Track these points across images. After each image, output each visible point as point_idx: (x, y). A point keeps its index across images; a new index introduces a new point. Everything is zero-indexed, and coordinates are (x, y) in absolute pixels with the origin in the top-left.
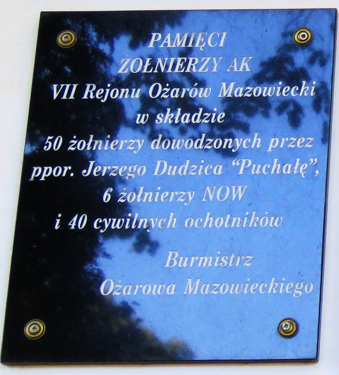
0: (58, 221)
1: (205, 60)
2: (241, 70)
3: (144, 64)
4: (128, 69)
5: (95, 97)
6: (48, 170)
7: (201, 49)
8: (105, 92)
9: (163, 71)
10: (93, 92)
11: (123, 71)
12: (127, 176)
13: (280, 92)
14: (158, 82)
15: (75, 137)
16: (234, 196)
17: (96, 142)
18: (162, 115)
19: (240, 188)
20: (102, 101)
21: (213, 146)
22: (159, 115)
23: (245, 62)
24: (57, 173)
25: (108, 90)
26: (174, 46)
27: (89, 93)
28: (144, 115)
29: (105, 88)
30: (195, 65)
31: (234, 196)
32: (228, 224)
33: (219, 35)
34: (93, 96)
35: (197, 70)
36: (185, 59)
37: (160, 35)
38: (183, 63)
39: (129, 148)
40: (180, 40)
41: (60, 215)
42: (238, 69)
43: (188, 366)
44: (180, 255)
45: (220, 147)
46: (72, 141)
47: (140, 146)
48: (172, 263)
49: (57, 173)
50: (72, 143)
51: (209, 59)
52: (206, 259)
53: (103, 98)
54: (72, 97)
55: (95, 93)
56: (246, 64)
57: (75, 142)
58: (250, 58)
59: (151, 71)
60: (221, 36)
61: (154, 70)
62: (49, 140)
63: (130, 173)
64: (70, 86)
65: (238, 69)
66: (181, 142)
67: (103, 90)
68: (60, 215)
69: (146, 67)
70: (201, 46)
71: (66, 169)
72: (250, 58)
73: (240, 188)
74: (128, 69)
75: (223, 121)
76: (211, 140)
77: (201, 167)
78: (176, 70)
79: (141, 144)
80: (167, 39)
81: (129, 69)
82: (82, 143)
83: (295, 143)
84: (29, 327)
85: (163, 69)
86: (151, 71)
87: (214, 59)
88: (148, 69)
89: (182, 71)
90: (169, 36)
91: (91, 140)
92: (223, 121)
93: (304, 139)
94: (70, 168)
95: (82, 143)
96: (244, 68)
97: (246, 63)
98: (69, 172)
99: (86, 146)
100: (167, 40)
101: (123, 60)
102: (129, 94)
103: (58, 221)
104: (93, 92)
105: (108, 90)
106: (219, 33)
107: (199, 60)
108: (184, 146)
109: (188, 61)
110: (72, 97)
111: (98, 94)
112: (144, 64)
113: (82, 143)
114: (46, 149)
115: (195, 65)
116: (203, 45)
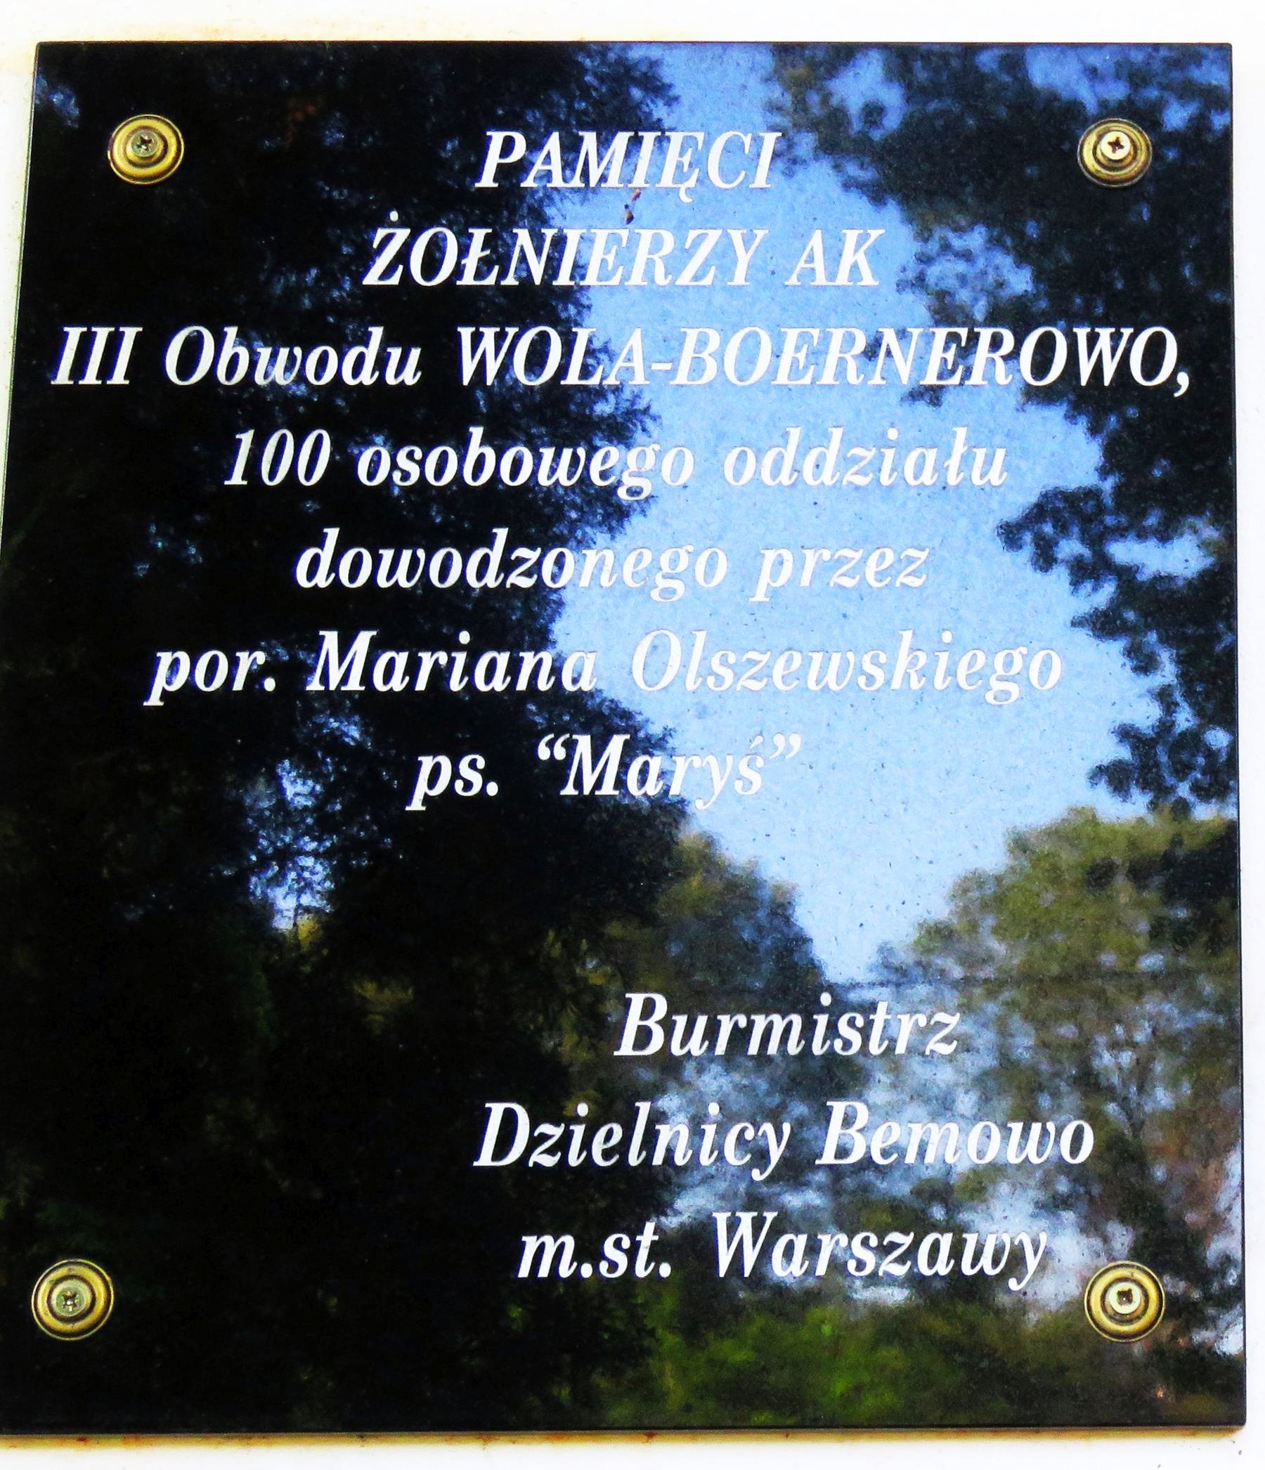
2: (843, 278)
3: (463, 251)
4: (401, 268)
7: (685, 198)
9: (537, 281)
11: (382, 277)
12: (989, 689)
14: (199, 324)
18: (418, 454)
21: (863, 578)
22: (406, 450)
23: (856, 251)
24: (209, 679)
28: (567, 453)
30: (664, 258)
33: (747, 140)
35: (670, 277)
37: (520, 141)
39: (836, 579)
42: (832, 276)
43: (270, 1444)
44: (673, 1010)
45: (453, 582)
48: (644, 1036)
49: (209, 679)
51: (714, 236)
52: (779, 1023)
54: (119, 378)
56: (862, 260)
59: (491, 280)
61: (503, 274)
63: (1000, 679)
65: (832, 276)
66: (414, 561)
69: (471, 264)
70: (683, 187)
74: (401, 268)
76: (531, 555)
77: (944, 658)
81: (407, 274)
82: (449, 557)
84: (48, 1291)
85: (537, 270)
86: (491, 280)
87: (737, 236)
90: (553, 143)
93: (890, 557)
94: (261, 657)
98: (255, 677)
101: (381, 233)
106: (750, 136)
107: (680, 239)
110: (119, 378)
112: (463, 251)
115: (664, 258)
116: (692, 182)
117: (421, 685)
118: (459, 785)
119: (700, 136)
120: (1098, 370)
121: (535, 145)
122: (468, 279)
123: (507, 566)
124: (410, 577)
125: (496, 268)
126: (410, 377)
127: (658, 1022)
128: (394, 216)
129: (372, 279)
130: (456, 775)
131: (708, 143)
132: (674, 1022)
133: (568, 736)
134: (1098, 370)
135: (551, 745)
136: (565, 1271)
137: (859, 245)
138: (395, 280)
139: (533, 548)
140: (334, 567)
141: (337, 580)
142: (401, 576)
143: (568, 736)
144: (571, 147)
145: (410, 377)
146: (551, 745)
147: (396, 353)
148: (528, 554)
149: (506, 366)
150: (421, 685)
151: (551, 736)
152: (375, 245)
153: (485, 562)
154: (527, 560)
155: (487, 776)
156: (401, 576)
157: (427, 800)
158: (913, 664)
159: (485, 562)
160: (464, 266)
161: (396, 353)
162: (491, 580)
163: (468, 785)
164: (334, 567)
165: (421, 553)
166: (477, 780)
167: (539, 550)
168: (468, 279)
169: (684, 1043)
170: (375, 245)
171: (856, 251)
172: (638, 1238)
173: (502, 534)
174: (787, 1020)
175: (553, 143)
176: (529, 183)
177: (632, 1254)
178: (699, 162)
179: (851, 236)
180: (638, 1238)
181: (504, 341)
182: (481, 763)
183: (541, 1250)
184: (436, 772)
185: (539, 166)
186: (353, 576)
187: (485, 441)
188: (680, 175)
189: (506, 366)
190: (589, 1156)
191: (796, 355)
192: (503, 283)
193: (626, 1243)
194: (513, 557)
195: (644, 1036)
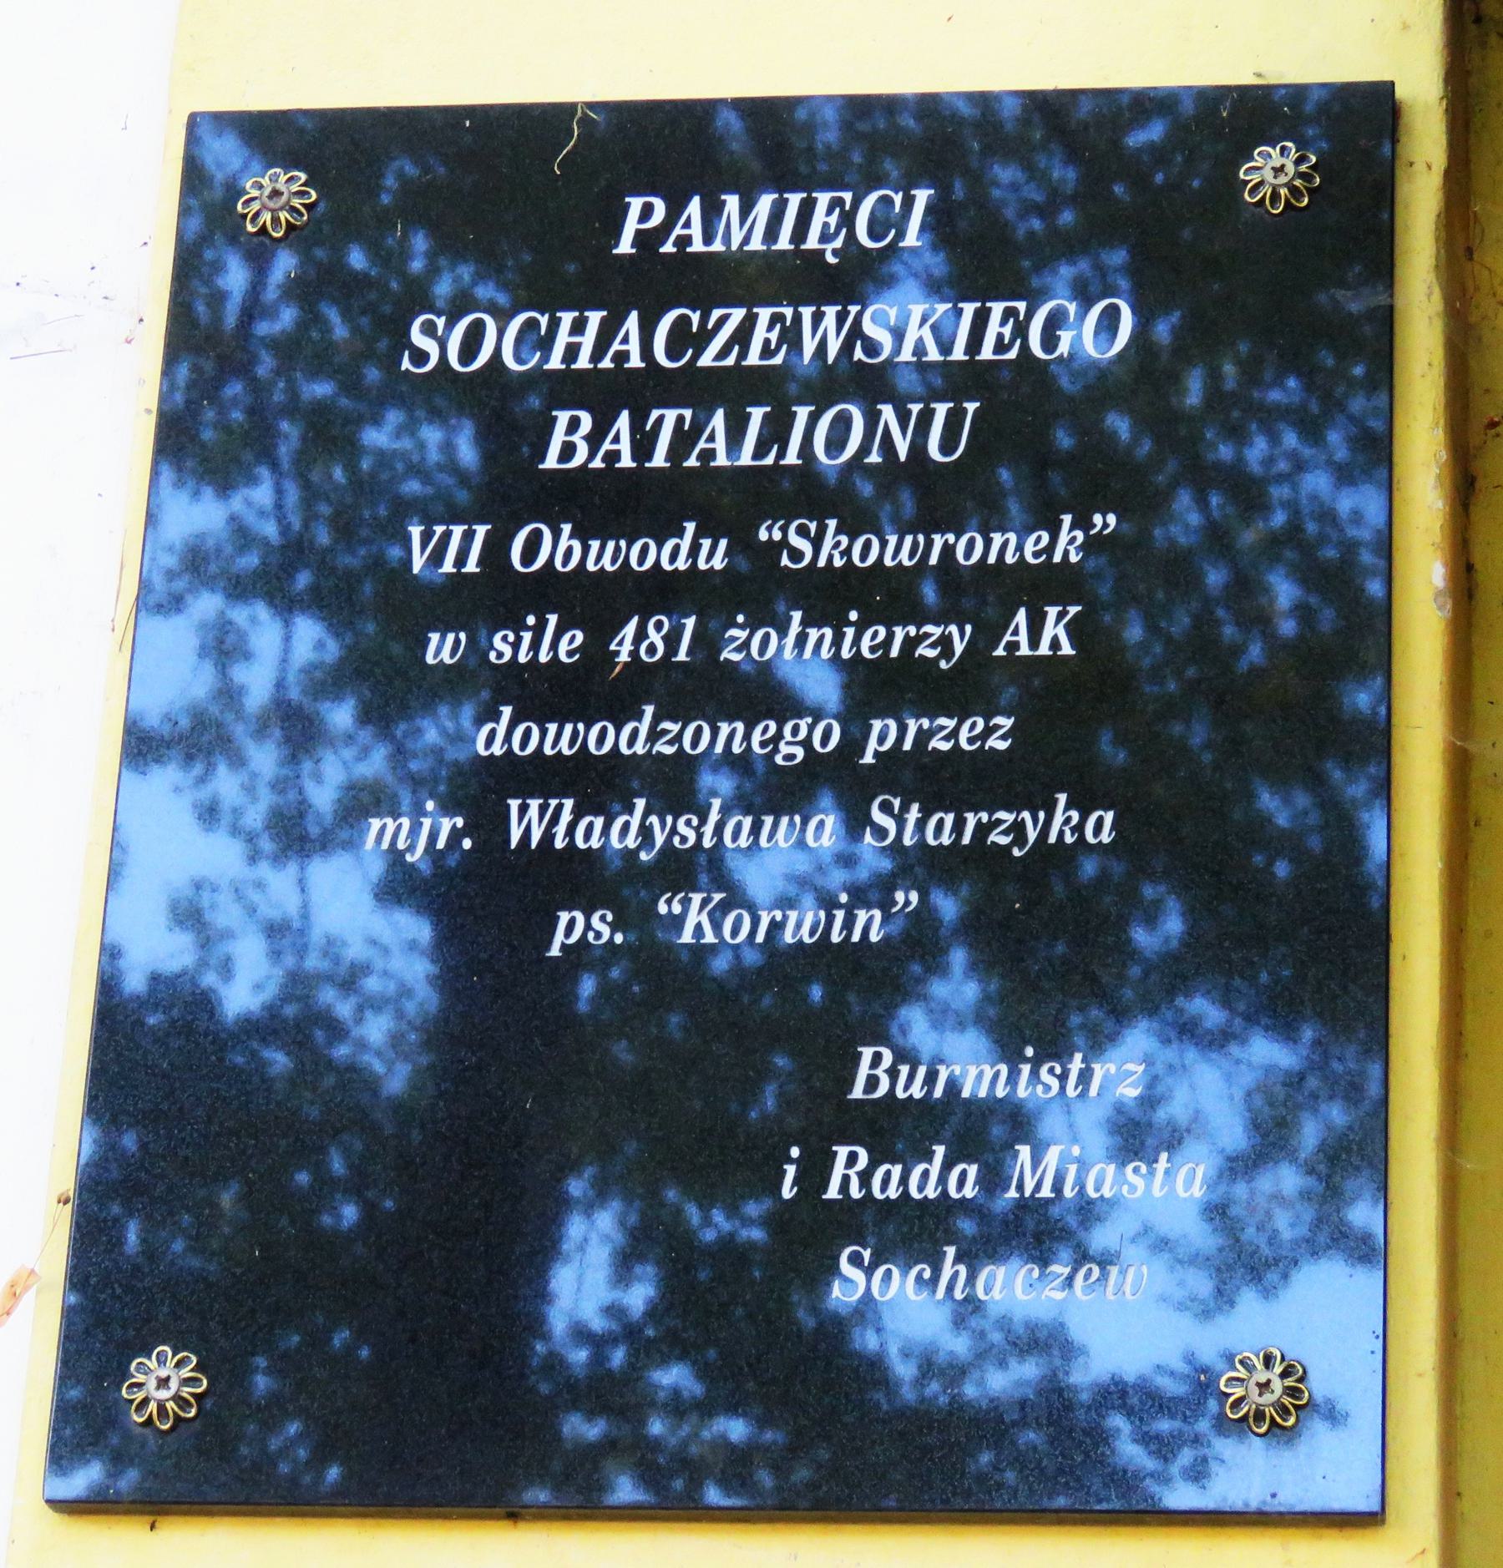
0: (791, 1170)
1: (723, 320)
2: (1044, 649)
15: (740, 619)
17: (813, 634)
23: (921, 326)
26: (717, 246)
30: (858, 1173)
40: (742, 224)
41: (795, 1152)
46: (734, 632)
47: (959, 648)
48: (872, 1083)
50: (734, 639)
54: (471, 567)
55: (865, 1178)
56: (1061, 632)
57: (742, 634)
58: (1073, 610)
60: (909, 202)
64: (979, 353)
66: (575, 733)
68: (795, 1152)
70: (829, 247)
72: (1073, 610)
75: (577, 656)
76: (673, 727)
79: (962, 639)
83: (954, 734)
86: (769, 460)
90: (694, 207)
91: (795, 628)
92: (577, 656)
95: (767, 637)
96: (1055, 644)
97: (927, 328)
99: (780, 649)
103: (791, 1170)
110: (471, 567)
113: (767, 637)
115: (858, 1173)
117: (966, 840)
118: (591, 935)
119: (848, 196)
120: (822, 347)
121: (675, 210)
123: (654, 735)
124: (571, 746)
126: (718, 563)
127: (886, 1071)
129: (706, 360)
130: (588, 927)
131: (1030, 314)
132: (899, 1071)
133: (683, 894)
134: (822, 347)
137: (924, 320)
139: (676, 722)
142: (564, 745)
143: (683, 894)
144: (712, 211)
145: (718, 563)
147: (706, 543)
149: (872, 418)
150: (966, 840)
153: (634, 734)
154: (932, 635)
155: (614, 927)
156: (564, 745)
157: (564, 946)
159: (634, 734)
161: (706, 543)
162: (640, 748)
163: (598, 935)
164: (508, 738)
165: (581, 726)
166: (606, 932)
167: (680, 724)
169: (906, 1088)
171: (921, 326)
174: (995, 1069)
175: (694, 207)
176: (668, 248)
178: (848, 220)
179: (1052, 612)
182: (610, 918)
184: (571, 924)
186: (523, 746)
188: (825, 237)
189: (872, 418)
191: (1002, 330)
195: (872, 1083)
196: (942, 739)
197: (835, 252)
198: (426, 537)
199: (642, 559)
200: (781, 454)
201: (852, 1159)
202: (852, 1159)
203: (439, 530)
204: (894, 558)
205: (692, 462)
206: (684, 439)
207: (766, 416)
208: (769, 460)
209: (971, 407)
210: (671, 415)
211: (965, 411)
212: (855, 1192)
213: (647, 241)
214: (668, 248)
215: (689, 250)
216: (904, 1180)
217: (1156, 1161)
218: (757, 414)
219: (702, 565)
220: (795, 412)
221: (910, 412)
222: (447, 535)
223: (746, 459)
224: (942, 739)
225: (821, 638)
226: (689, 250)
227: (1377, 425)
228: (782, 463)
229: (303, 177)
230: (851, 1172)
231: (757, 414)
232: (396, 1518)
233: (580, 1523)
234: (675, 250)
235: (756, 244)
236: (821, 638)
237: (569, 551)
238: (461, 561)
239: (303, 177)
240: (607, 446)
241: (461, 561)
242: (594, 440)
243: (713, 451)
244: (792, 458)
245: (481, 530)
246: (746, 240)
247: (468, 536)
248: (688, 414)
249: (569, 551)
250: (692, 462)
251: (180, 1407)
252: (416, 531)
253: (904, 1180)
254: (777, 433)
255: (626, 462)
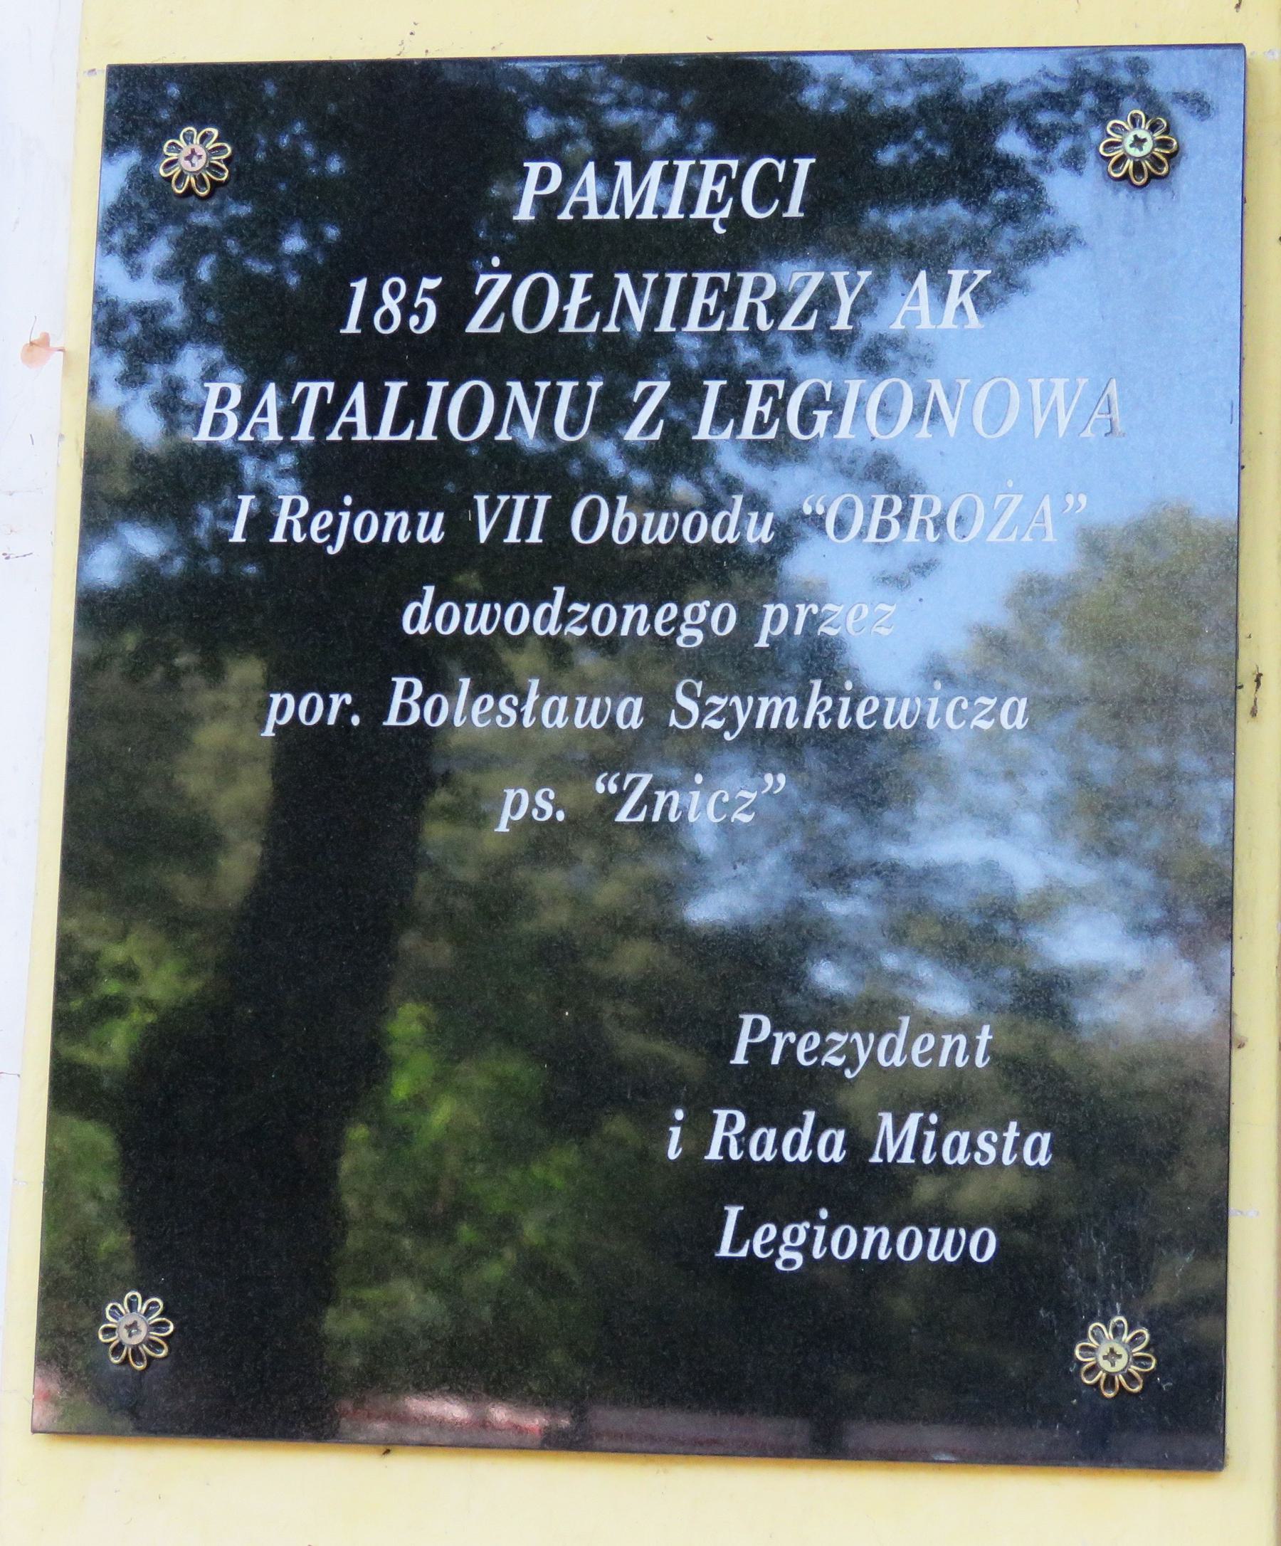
0: (676, 1132)
4: (503, 315)
5: (309, 538)
6: (283, 705)
7: (719, 230)
8: (337, 520)
10: (301, 520)
13: (929, 1461)
16: (1040, 421)
19: (1060, 384)
20: (330, 551)
23: (963, 290)
25: (345, 516)
26: (612, 215)
27: (290, 525)
29: (337, 507)
31: (1040, 421)
32: (935, 720)
34: (302, 535)
36: (726, 277)
38: (716, 292)
40: (635, 191)
41: (679, 1115)
53: (332, 542)
54: (534, 538)
55: (306, 523)
56: (967, 299)
58: (981, 274)
59: (592, 327)
60: (792, 171)
61: (604, 321)
62: (427, 293)
67: (330, 517)
68: (679, 1115)
69: (573, 309)
70: (717, 217)
71: (336, 700)
73: (1060, 384)
74: (503, 315)
78: (693, 324)
80: (353, 406)
81: (509, 320)
86: (406, 436)
88: (583, 319)
89: (717, 326)
98: (345, 711)
100: (352, 413)
102: (409, 528)
103: (676, 1132)
104: (301, 520)
105: (345, 516)
108: (502, 622)
109: (736, 284)
110: (534, 538)
111: (315, 527)
112: (565, 297)
114: (418, 327)
118: (535, 813)
119: (734, 164)
121: (571, 176)
122: (570, 326)
123: (565, 617)
125: (598, 314)
126: (436, 536)
128: (496, 262)
130: (533, 804)
135: (605, 782)
136: (883, 1255)
138: (497, 328)
140: (431, 618)
141: (433, 628)
145: (436, 536)
146: (605, 782)
148: (581, 608)
149: (502, 396)
151: (606, 774)
152: (477, 292)
154: (581, 613)
157: (511, 823)
158: (822, 706)
160: (566, 312)
163: (542, 812)
164: (431, 618)
165: (498, 607)
168: (570, 326)
170: (477, 292)
172: (1005, 1135)
173: (560, 591)
176: (565, 215)
177: (1000, 1146)
178: (734, 189)
179: (957, 275)
180: (1005, 1135)
181: (932, 410)
182: (552, 796)
183: (772, 708)
185: (574, 198)
187: (628, 508)
188: (714, 206)
189: (502, 396)
190: (829, 1250)
192: (605, 330)
193: (995, 1138)
194: (569, 610)
196: (714, 717)
197: (723, 223)
198: (491, 506)
199: (694, 531)
200: (417, 431)
201: (731, 1121)
202: (731, 1121)
203: (503, 499)
204: (651, 536)
205: (334, 436)
206: (326, 415)
207: (403, 390)
208: (406, 436)
209: (595, 386)
210: (314, 388)
211: (589, 389)
212: (735, 1154)
213: (549, 205)
214: (565, 215)
215: (585, 217)
216: (778, 1143)
217: (1006, 1130)
218: (395, 389)
219: (421, 539)
220: (750, 386)
221: (538, 389)
222: (510, 505)
223: (384, 434)
224: (714, 717)
225: (638, 615)
226: (585, 217)
227: (698, 411)
228: (418, 438)
229: (215, 132)
230: (730, 1135)
231: (395, 389)
232: (1022, 1464)
233: (555, 1453)
234: (571, 217)
235: (674, 213)
236: (638, 615)
237: (625, 524)
238: (525, 530)
239: (215, 132)
240: (255, 419)
241: (525, 530)
242: (246, 410)
243: (266, 425)
244: (427, 434)
245: (543, 501)
246: (899, 1154)
247: (530, 508)
248: (330, 386)
249: (625, 524)
250: (334, 436)
251: (158, 1331)
252: (481, 500)
253: (778, 1143)
254: (412, 408)
255: (362, 435)
